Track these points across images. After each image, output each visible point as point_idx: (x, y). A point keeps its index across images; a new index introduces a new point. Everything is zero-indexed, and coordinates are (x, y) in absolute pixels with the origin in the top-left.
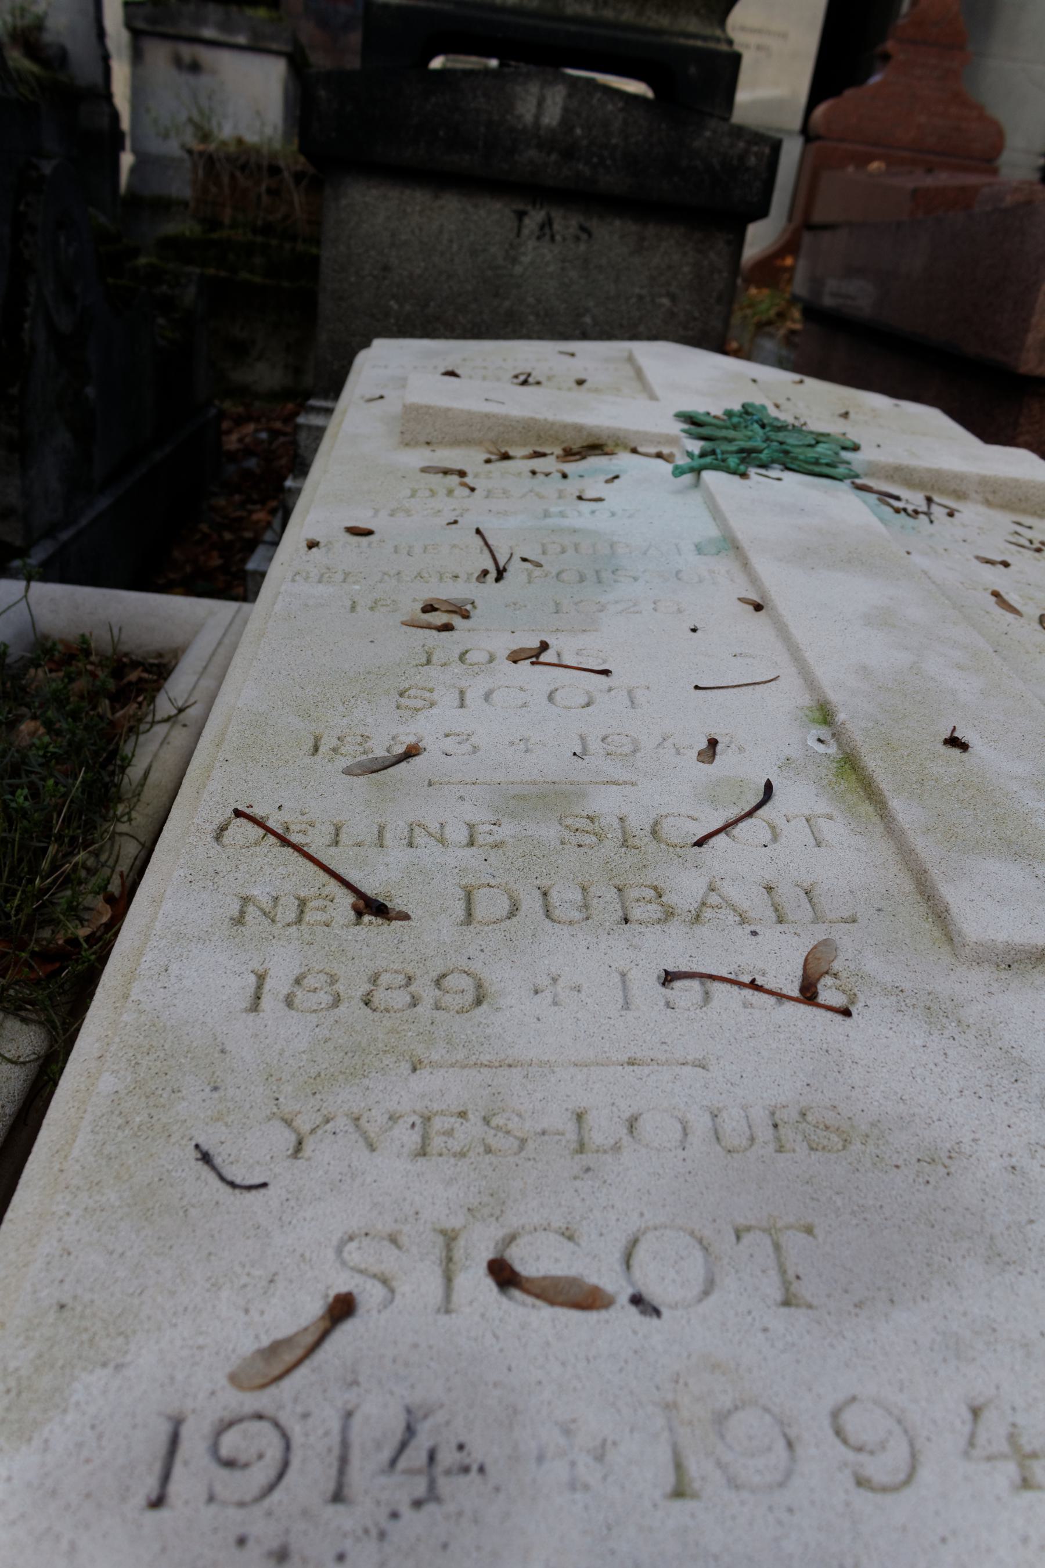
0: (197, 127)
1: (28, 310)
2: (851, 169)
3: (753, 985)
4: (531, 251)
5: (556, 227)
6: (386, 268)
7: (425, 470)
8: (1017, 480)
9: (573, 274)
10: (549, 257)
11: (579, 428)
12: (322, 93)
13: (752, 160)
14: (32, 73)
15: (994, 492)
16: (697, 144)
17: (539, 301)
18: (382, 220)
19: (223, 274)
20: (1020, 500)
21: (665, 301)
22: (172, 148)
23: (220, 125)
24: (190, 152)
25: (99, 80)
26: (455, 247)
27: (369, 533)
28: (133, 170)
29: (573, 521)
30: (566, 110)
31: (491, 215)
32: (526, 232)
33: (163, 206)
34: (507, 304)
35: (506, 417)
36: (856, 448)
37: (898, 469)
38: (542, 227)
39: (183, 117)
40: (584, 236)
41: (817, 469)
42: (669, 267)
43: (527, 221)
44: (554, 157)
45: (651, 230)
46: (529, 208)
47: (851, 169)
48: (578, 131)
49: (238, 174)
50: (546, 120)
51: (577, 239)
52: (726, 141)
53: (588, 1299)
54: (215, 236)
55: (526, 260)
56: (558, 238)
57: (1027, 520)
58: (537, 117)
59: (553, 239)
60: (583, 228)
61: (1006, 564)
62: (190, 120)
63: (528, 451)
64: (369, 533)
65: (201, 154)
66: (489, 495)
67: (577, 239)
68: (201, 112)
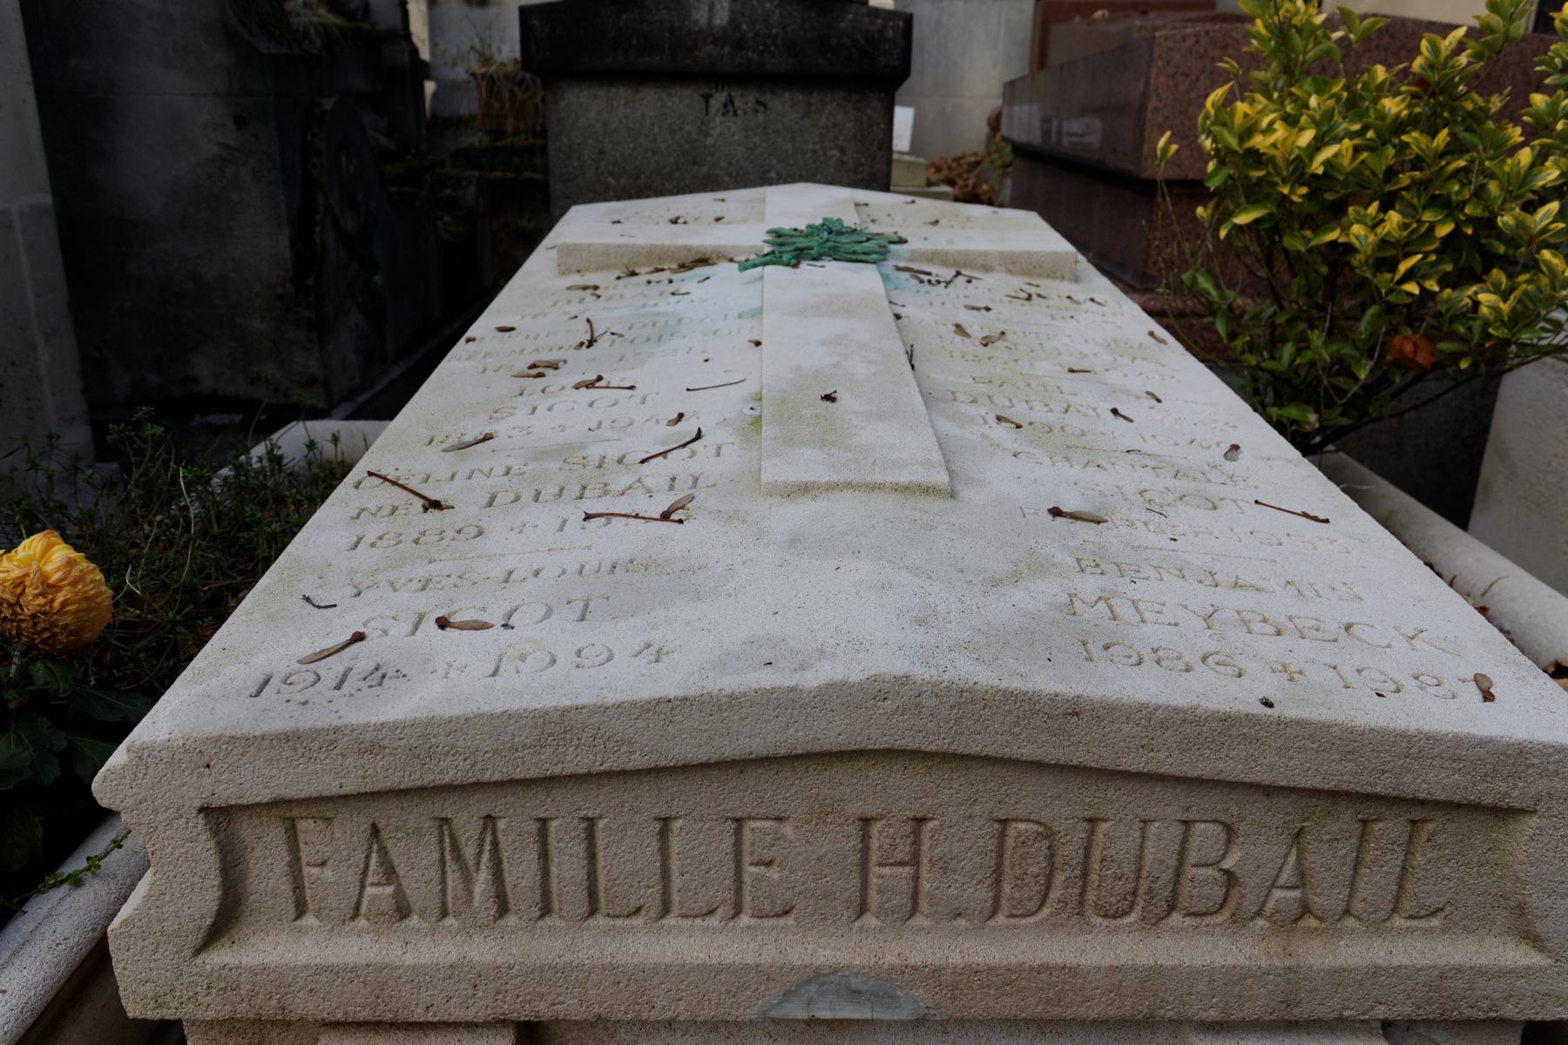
0: (481, 54)
1: (318, 217)
2: (1077, 19)
3: (637, 516)
5: (737, 103)
6: (602, 152)
7: (569, 288)
8: (1028, 253)
9: (756, 140)
10: (734, 129)
11: (688, 249)
12: (536, 22)
13: (890, 33)
14: (337, 26)
16: (842, 25)
17: (730, 164)
18: (592, 113)
19: (509, 175)
21: (835, 153)
22: (460, 73)
23: (499, 51)
24: (473, 75)
25: (399, 23)
26: (656, 129)
27: (512, 329)
28: (435, 96)
29: (662, 308)
30: (732, 11)
31: (682, 102)
32: (712, 111)
33: (457, 123)
34: (705, 169)
35: (634, 246)
36: (902, 241)
37: (935, 253)
38: (725, 105)
39: (466, 47)
40: (761, 109)
42: (835, 125)
43: (712, 102)
44: (727, 49)
45: (815, 97)
47: (1077, 19)
48: (745, 27)
49: (516, 89)
50: (717, 22)
51: (756, 111)
52: (866, 20)
53: (483, 626)
54: (500, 144)
55: (716, 132)
58: (710, 20)
59: (735, 114)
60: (759, 102)
61: (988, 309)
62: (472, 48)
63: (651, 268)
64: (512, 329)
65: (483, 76)
66: (610, 298)
68: (482, 41)
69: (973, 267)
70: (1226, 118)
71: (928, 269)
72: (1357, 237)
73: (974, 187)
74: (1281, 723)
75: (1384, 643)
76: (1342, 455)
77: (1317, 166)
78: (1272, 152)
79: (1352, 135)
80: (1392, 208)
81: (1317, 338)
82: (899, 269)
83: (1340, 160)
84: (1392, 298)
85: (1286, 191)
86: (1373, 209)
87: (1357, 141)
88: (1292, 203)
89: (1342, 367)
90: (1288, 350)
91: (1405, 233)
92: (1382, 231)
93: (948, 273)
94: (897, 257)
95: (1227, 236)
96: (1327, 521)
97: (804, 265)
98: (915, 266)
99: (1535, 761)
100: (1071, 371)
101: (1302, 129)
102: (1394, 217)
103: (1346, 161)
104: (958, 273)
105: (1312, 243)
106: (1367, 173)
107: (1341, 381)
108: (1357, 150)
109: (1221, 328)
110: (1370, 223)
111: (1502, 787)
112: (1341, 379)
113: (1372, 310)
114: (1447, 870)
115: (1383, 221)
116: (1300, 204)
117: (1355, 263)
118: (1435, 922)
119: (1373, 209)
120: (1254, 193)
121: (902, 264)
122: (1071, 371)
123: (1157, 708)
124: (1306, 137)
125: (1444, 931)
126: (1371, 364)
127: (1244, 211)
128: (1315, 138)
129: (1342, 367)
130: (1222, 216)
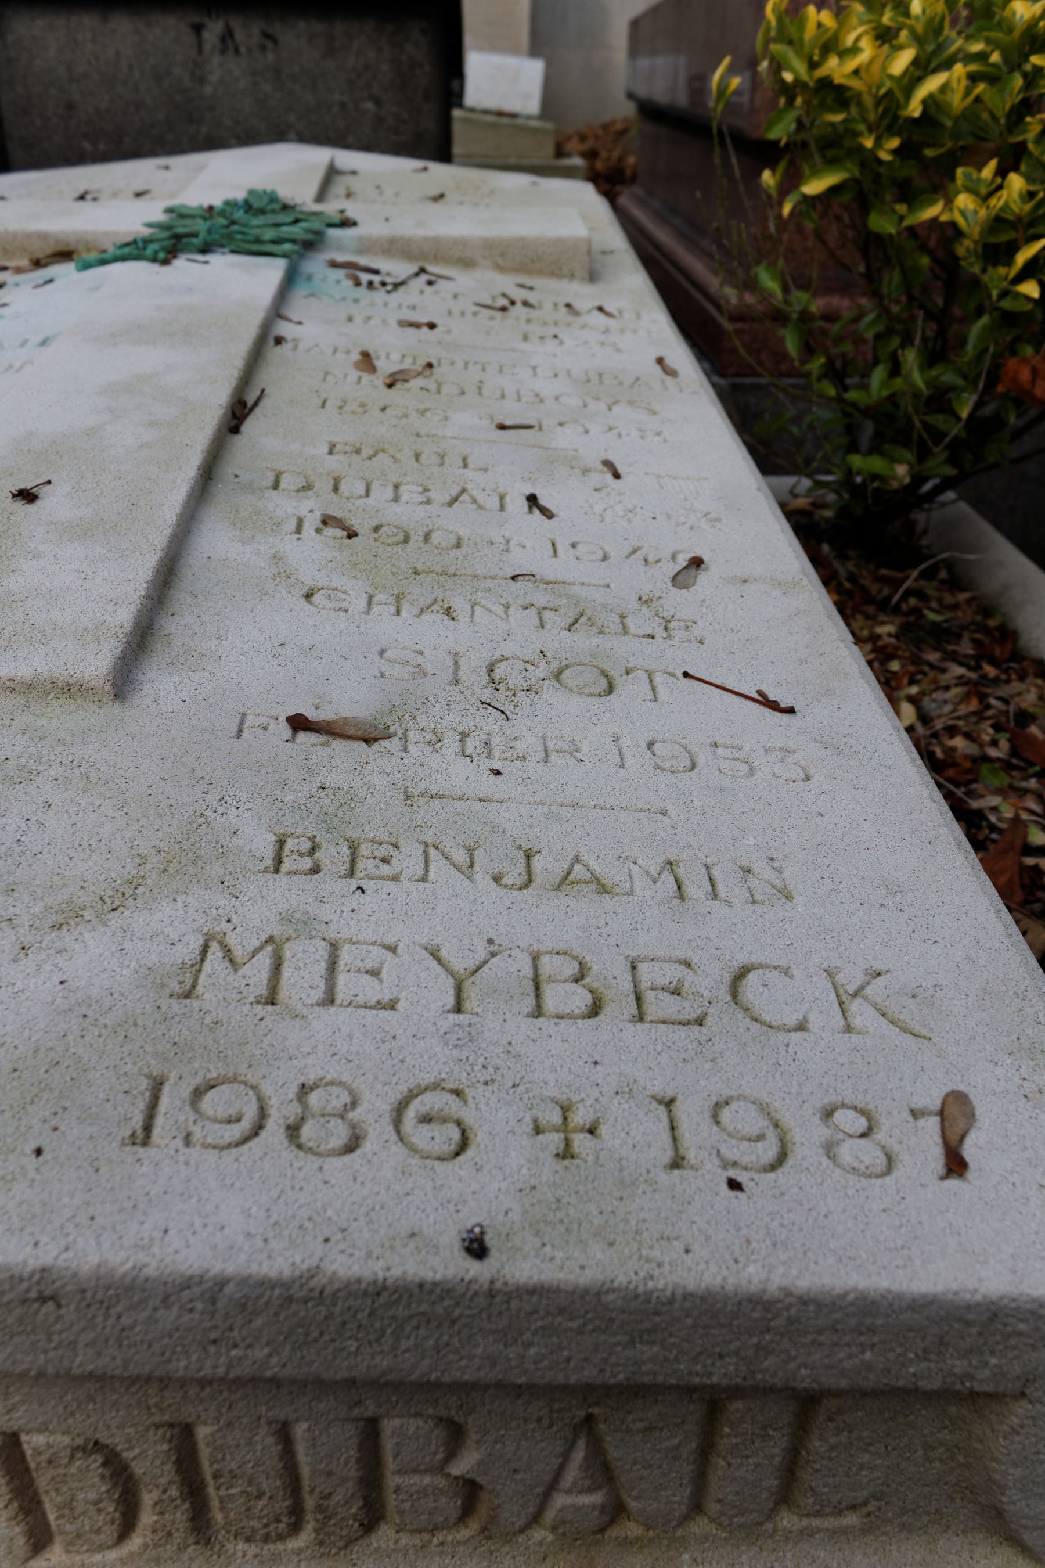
4: (217, 68)
5: (239, 36)
6: (70, 106)
8: (522, 239)
11: (44, 236)
15: (502, 255)
20: (532, 260)
21: (369, 106)
26: (137, 74)
32: (207, 47)
34: (204, 130)
36: (346, 223)
38: (223, 39)
40: (270, 44)
41: (255, 247)
43: (206, 35)
45: (339, 28)
46: (205, 20)
51: (263, 48)
55: (214, 78)
56: (243, 50)
57: (528, 281)
59: (237, 51)
61: (432, 326)
67: (263, 48)
69: (437, 259)
70: (792, 31)
71: (374, 265)
72: (963, 213)
73: (621, 159)
74: (497, 1297)
75: (791, 1021)
76: (963, 506)
77: (914, 108)
78: (856, 84)
79: (970, 58)
80: (1016, 169)
81: (910, 357)
82: (334, 265)
83: (948, 97)
84: (1006, 304)
85: (869, 143)
86: (988, 171)
87: (973, 67)
88: (880, 162)
89: (939, 400)
90: (879, 374)
91: (1028, 207)
92: (997, 202)
93: (400, 269)
94: (340, 248)
95: (792, 213)
96: (791, 711)
97: (181, 263)
98: (363, 261)
99: (1022, 1327)
100: (502, 427)
101: (901, 48)
102: (1016, 182)
103: (957, 101)
104: (423, 270)
105: (906, 223)
106: (985, 116)
107: (938, 420)
108: (973, 78)
109: (791, 345)
110: (983, 191)
111: (959, 1366)
112: (941, 417)
113: (985, 320)
114: (866, 1457)
115: (1000, 187)
116: (889, 163)
117: (961, 251)
118: (852, 1520)
119: (988, 171)
120: (834, 147)
121: (341, 258)
122: (502, 427)
123: (222, 1282)
124: (902, 61)
125: (865, 1531)
126: (974, 398)
127: (816, 173)
128: (915, 62)
129: (939, 400)
130: (790, 182)
